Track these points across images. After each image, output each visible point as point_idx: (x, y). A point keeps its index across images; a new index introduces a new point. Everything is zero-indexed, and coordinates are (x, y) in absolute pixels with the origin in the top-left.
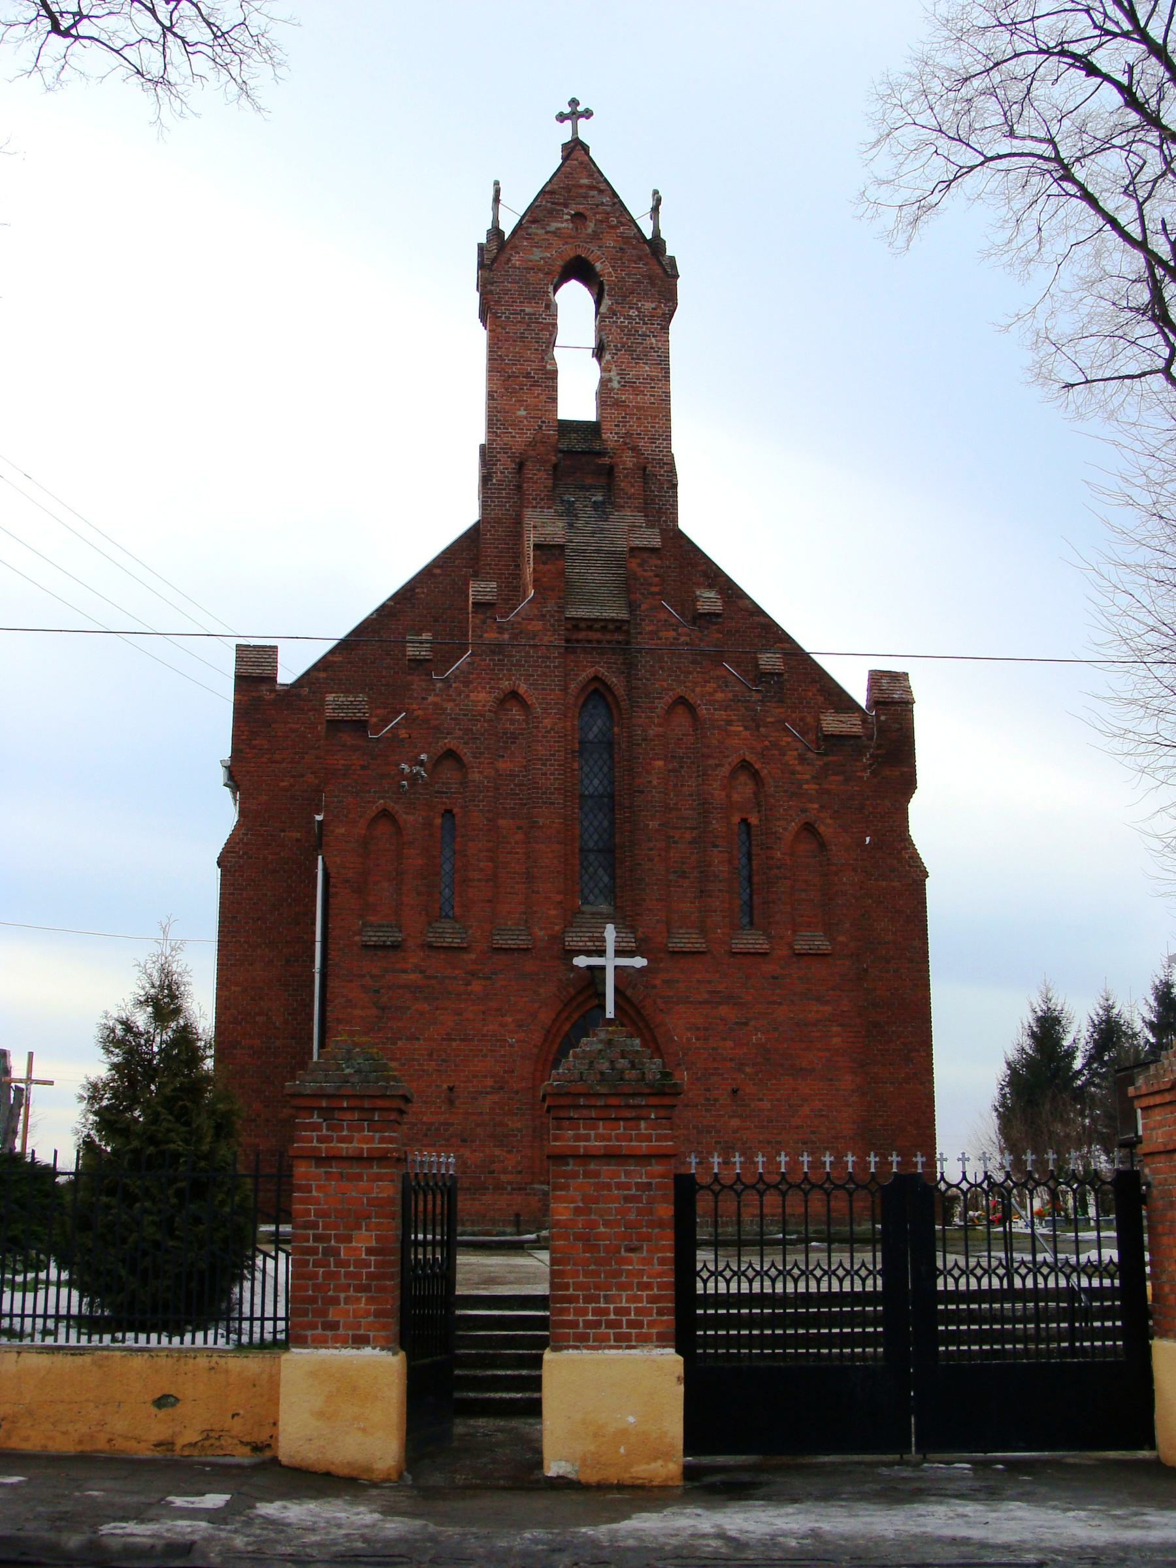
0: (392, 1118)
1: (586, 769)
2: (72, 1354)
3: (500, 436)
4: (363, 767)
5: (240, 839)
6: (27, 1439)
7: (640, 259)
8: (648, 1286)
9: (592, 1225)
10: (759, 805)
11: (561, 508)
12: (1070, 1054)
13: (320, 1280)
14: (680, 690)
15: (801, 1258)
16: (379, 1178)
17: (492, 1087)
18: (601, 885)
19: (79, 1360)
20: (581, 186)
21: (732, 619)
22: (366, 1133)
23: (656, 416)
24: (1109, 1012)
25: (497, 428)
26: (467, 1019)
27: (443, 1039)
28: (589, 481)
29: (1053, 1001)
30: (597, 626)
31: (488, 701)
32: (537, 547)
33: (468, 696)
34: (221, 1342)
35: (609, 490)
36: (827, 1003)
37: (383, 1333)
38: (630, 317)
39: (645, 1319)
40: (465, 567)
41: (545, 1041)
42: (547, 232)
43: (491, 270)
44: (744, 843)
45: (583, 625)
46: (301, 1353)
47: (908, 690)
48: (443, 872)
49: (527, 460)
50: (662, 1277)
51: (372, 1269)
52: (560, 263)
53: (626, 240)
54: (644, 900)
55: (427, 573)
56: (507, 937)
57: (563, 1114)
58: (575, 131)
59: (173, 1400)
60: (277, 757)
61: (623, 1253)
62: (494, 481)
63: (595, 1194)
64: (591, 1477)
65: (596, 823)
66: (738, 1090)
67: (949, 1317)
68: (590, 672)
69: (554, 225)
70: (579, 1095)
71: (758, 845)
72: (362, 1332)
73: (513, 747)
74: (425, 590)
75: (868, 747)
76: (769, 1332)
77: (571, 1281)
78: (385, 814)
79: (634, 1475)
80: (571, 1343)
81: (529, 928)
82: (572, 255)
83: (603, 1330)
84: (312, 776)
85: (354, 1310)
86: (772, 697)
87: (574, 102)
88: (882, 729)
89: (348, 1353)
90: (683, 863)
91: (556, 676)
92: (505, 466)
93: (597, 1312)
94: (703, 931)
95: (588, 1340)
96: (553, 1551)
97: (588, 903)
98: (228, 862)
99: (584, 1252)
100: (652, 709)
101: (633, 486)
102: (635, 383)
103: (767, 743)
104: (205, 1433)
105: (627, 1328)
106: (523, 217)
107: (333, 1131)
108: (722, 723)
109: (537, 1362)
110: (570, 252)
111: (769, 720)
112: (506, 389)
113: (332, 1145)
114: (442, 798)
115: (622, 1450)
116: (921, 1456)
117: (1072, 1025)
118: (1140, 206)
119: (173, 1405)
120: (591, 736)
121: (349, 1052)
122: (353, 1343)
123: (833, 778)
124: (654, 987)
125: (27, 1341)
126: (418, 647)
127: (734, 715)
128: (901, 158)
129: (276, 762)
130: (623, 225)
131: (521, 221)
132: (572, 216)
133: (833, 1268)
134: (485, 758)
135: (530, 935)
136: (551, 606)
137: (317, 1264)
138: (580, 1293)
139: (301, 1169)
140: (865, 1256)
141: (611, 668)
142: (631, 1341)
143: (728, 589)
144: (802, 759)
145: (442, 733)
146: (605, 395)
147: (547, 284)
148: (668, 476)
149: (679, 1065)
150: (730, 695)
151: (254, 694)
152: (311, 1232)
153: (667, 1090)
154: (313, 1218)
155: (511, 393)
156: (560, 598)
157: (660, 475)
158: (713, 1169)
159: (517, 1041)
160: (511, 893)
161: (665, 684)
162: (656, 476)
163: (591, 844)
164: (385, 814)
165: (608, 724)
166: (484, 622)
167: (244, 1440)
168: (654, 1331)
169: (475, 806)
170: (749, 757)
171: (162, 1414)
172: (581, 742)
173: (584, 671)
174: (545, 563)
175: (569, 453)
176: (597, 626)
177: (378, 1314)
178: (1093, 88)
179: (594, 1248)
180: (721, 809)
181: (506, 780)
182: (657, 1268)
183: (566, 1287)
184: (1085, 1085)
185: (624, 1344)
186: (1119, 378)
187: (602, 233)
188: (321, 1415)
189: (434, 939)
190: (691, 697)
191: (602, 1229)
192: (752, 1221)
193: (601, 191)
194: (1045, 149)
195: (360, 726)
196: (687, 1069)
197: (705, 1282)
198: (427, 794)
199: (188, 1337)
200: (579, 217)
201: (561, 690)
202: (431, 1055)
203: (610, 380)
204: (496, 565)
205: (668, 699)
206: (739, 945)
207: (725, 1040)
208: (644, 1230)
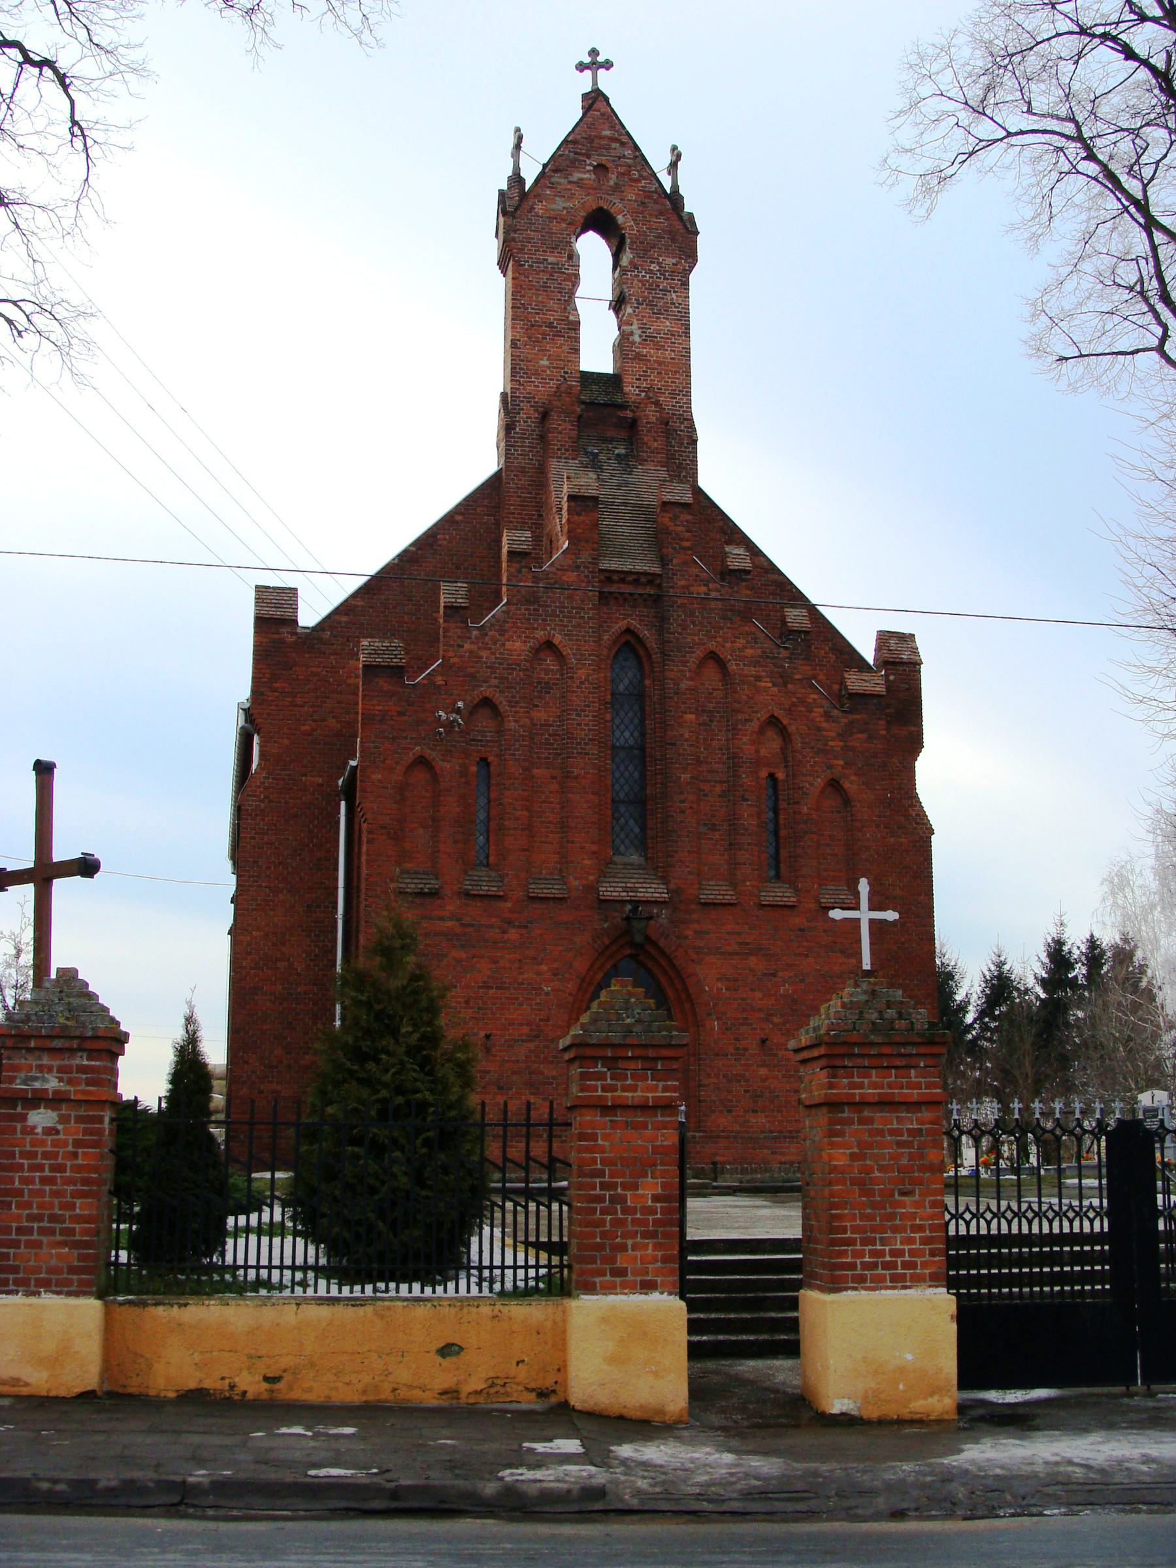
1: (618, 721)
2: (353, 1305)
4: (400, 714)
5: (261, 783)
6: (310, 1390)
7: (661, 213)
8: (920, 1228)
9: (868, 1170)
10: (786, 760)
12: (963, 1008)
13: (608, 1227)
14: (712, 645)
15: (1055, 1201)
18: (632, 836)
19: (361, 1311)
22: (649, 1082)
23: (676, 372)
24: (1000, 968)
25: (521, 377)
26: (504, 968)
27: (480, 988)
29: (946, 957)
30: (630, 578)
31: (524, 651)
32: (571, 498)
33: (503, 645)
34: (474, 1289)
35: (632, 444)
38: (651, 272)
39: (919, 1260)
41: (579, 990)
42: (570, 182)
43: (514, 218)
45: (615, 577)
47: (915, 651)
48: (478, 821)
49: (552, 410)
50: (932, 1220)
51: (659, 1216)
52: (583, 214)
53: (648, 194)
54: (676, 852)
55: (449, 521)
56: (543, 886)
57: (838, 1063)
59: (457, 1348)
60: (299, 700)
61: (896, 1196)
64: (873, 1413)
65: (627, 774)
67: (1101, 1258)
68: (621, 625)
69: (577, 176)
70: (855, 1044)
71: (784, 800)
74: (447, 537)
77: (848, 1224)
81: (564, 877)
83: (880, 1271)
84: (334, 721)
87: (594, 52)
90: (713, 816)
92: (527, 416)
93: (874, 1253)
94: (734, 885)
97: (620, 854)
99: (860, 1196)
100: (684, 663)
101: (655, 440)
103: (795, 700)
104: (491, 1381)
106: (545, 166)
108: (752, 679)
109: (794, 1304)
110: (592, 203)
111: (797, 677)
112: (529, 338)
114: (477, 746)
115: (901, 1387)
117: (965, 980)
119: (458, 1353)
120: (621, 687)
121: (627, 1002)
122: (641, 1289)
124: (686, 937)
125: (287, 1293)
127: (763, 671)
129: (296, 705)
132: (595, 167)
134: (521, 707)
135: (565, 884)
136: (585, 558)
137: (604, 1211)
141: (643, 620)
144: (827, 716)
146: (623, 348)
147: (569, 235)
148: (688, 432)
149: (710, 1014)
150: (759, 651)
152: (598, 1180)
153: (937, 1040)
154: (599, 1166)
155: (534, 342)
156: (593, 550)
157: (681, 431)
160: (545, 843)
161: (696, 638)
162: (676, 431)
163: (622, 795)
165: (638, 676)
167: (529, 1387)
168: (927, 1271)
171: (447, 1362)
172: (613, 694)
173: (616, 623)
174: (579, 514)
176: (630, 578)
177: (665, 1260)
179: (869, 1193)
180: (751, 763)
181: (541, 729)
184: (975, 1039)
186: (1113, 353)
188: (613, 1360)
189: (470, 887)
190: (726, 655)
191: (877, 1174)
192: (780, 1168)
193: (623, 144)
195: (397, 672)
196: (718, 1019)
198: (463, 742)
199: (451, 1286)
200: (601, 168)
202: (467, 1002)
204: (519, 514)
205: (700, 653)
207: (752, 990)
208: (916, 1175)
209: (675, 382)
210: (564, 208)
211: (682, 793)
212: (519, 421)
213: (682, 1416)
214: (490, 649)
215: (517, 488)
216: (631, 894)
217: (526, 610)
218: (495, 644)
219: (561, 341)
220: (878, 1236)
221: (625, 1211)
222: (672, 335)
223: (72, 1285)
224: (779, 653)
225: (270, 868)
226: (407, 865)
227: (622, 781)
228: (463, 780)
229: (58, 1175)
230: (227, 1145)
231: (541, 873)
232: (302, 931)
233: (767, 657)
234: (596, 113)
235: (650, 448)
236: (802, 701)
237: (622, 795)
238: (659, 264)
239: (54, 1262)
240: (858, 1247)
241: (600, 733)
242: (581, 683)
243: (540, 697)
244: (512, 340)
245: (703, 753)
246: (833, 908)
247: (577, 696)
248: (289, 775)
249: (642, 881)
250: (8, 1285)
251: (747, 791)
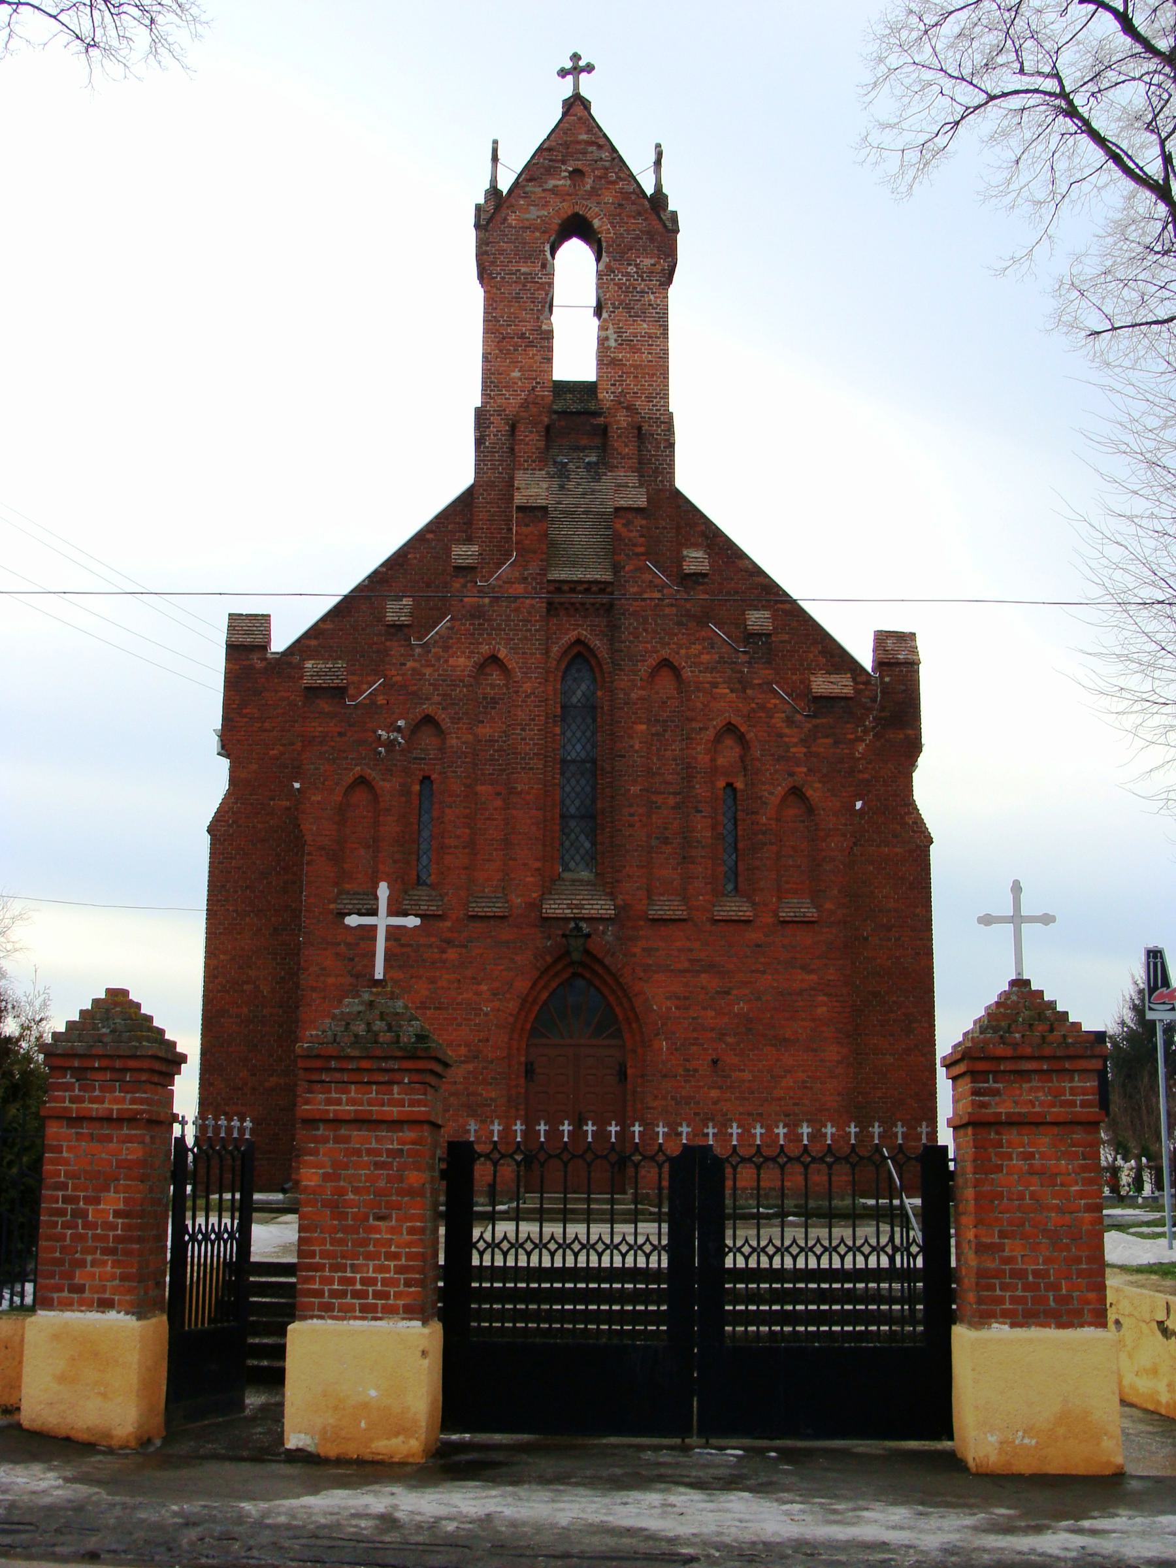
0: (144, 1078)
1: (569, 734)
3: (493, 398)
4: (340, 734)
7: (640, 214)
8: (396, 1256)
9: (341, 1192)
10: (745, 769)
11: (552, 470)
13: (68, 1242)
14: (665, 653)
16: (129, 1139)
17: (465, 1056)
18: (582, 851)
20: (579, 142)
21: (732, 579)
23: (653, 375)
25: (491, 391)
28: (584, 442)
30: (580, 588)
31: (468, 666)
33: (447, 661)
36: (811, 972)
37: (128, 1298)
38: (628, 274)
40: (459, 532)
42: (544, 190)
43: (486, 230)
44: (729, 808)
45: (565, 587)
46: (46, 1316)
47: (914, 650)
51: (119, 1232)
53: (625, 195)
55: (419, 539)
56: (484, 904)
57: (315, 1077)
58: (576, 85)
60: (267, 725)
61: (371, 1220)
62: (487, 444)
63: (345, 1159)
64: (331, 1451)
65: (578, 789)
66: (717, 1060)
67: (736, 1298)
68: (572, 635)
69: (552, 183)
70: (331, 1057)
71: (743, 811)
72: (107, 1296)
73: (493, 712)
74: (418, 556)
75: (870, 710)
76: (630, 1308)
77: (317, 1248)
78: (362, 781)
79: (374, 1450)
80: (316, 1313)
81: (507, 895)
82: (570, 213)
83: (349, 1300)
86: (760, 658)
87: (576, 57)
88: (886, 690)
89: (94, 1316)
90: (666, 829)
91: (537, 640)
92: (498, 425)
93: (343, 1281)
95: (333, 1311)
96: (187, 1525)
97: (570, 870)
98: (218, 830)
99: (332, 1219)
101: (626, 446)
102: (632, 341)
103: (753, 705)
105: (373, 1299)
106: (520, 175)
107: (85, 1091)
108: (708, 685)
111: (756, 682)
112: (501, 351)
113: (83, 1105)
115: (363, 1425)
116: (704, 1441)
118: (1162, 143)
120: (574, 700)
124: (634, 955)
126: (398, 610)
127: (721, 677)
128: (906, 100)
129: (266, 731)
130: (622, 179)
131: (517, 179)
132: (571, 173)
133: (834, 1243)
137: (66, 1226)
139: (53, 1129)
140: (648, 1228)
141: (595, 630)
142: (377, 1312)
143: (728, 549)
145: (421, 699)
146: (605, 358)
149: (658, 1034)
150: (717, 657)
151: (244, 663)
152: (60, 1193)
153: (420, 1054)
154: (62, 1179)
157: (657, 434)
158: (802, 1141)
159: (492, 1010)
163: (573, 810)
164: (362, 781)
165: (592, 687)
166: (464, 586)
169: (453, 772)
170: (736, 720)
173: (567, 634)
174: (527, 525)
175: (564, 413)
176: (580, 588)
177: (124, 1278)
178: (1085, 20)
179: (342, 1216)
180: (705, 773)
182: (406, 1237)
183: (312, 1254)
185: (370, 1315)
186: (1147, 323)
187: (601, 189)
188: (61, 1379)
189: (409, 907)
191: (351, 1196)
193: (600, 147)
194: (1051, 85)
195: (339, 692)
196: (666, 1039)
197: (481, 1254)
201: (542, 654)
203: (607, 338)
205: (652, 661)
206: (721, 913)
207: (704, 1009)
210: (538, 217)
211: (631, 806)
213: (128, 1442)
214: (433, 666)
215: (487, 503)
217: (470, 625)
218: (439, 659)
221: (87, 1225)
222: (649, 337)
224: (738, 658)
225: (237, 892)
226: (347, 886)
227: (573, 795)
228: (404, 799)
230: (194, 1165)
231: (483, 891)
232: (269, 954)
233: (725, 662)
235: (620, 454)
236: (762, 707)
237: (573, 810)
238: (637, 265)
240: (327, 1274)
241: (546, 747)
242: (527, 696)
243: (485, 713)
245: (656, 764)
246: (350, 914)
247: (522, 711)
248: (257, 800)
249: (590, 897)
251: (700, 802)
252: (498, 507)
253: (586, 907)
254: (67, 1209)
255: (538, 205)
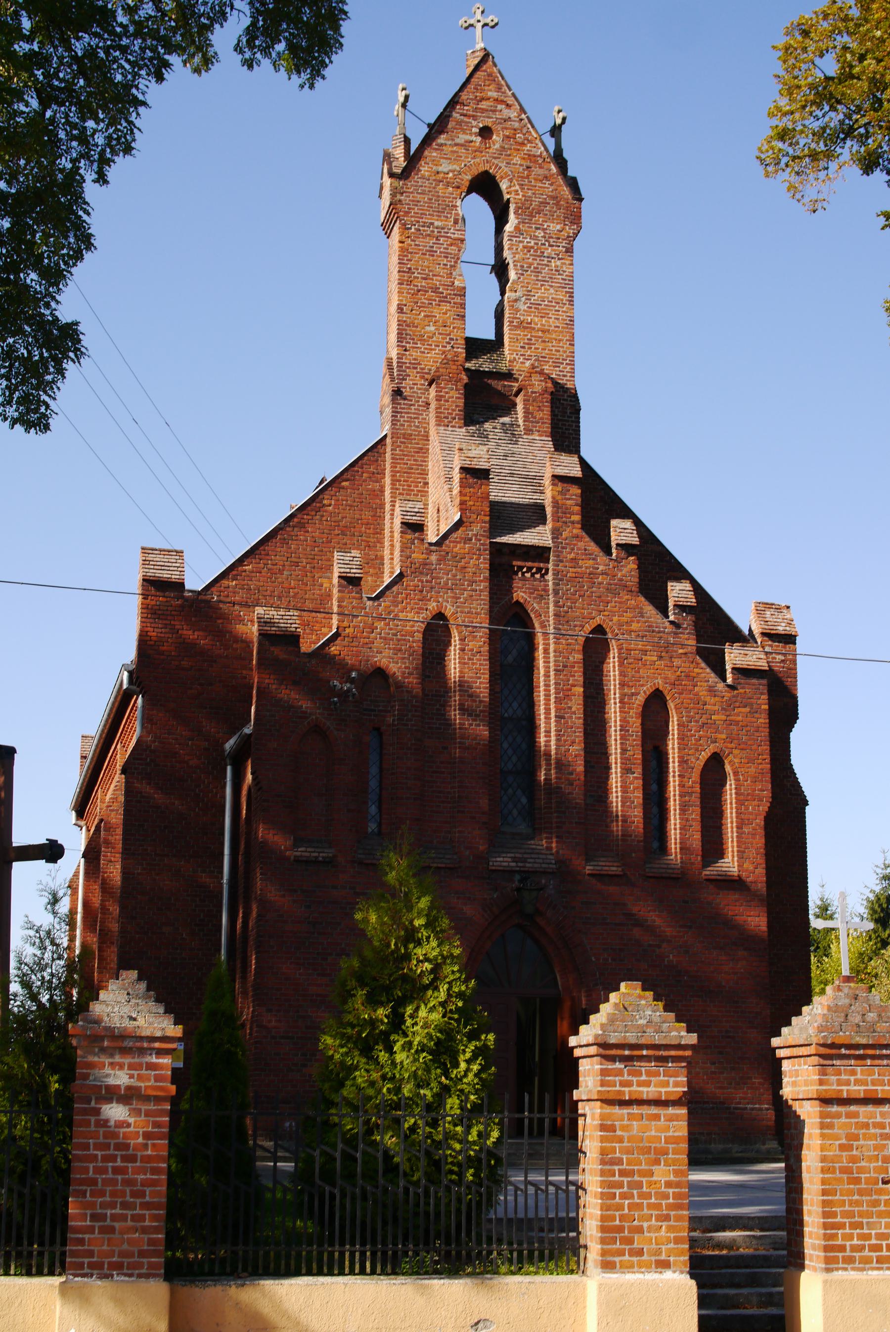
7: (546, 177)
9: (854, 1160)
13: (626, 1211)
23: (560, 340)
42: (456, 145)
52: (469, 177)
77: (838, 1210)
80: (841, 1265)
82: (482, 169)
85: (656, 1237)
89: (652, 1276)
93: (863, 1237)
95: (854, 1262)
102: (540, 305)
120: (510, 659)
122: (657, 1268)
123: (740, 709)
130: (530, 142)
137: (624, 1196)
138: (847, 1220)
154: (618, 1155)
155: (420, 307)
157: (564, 400)
193: (508, 106)
200: (486, 132)
209: (558, 351)
212: (405, 388)
216: (520, 864)
219: (445, 307)
220: (865, 1220)
221: (642, 1196)
223: (143, 1268)
229: (130, 1165)
234: (483, 73)
239: (125, 1247)
244: (398, 305)
248: (177, 739)
250: (83, 1268)
252: (415, 460)
253: (529, 860)
254: (623, 1181)
255: (450, 159)
